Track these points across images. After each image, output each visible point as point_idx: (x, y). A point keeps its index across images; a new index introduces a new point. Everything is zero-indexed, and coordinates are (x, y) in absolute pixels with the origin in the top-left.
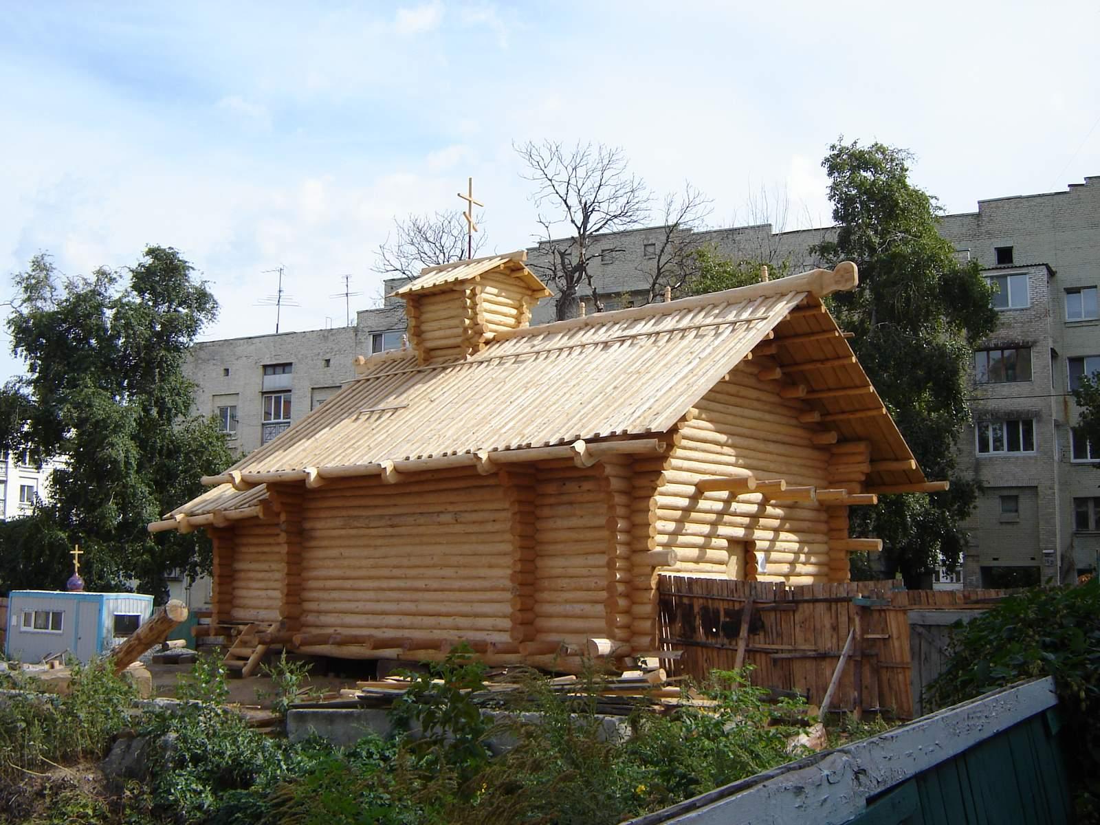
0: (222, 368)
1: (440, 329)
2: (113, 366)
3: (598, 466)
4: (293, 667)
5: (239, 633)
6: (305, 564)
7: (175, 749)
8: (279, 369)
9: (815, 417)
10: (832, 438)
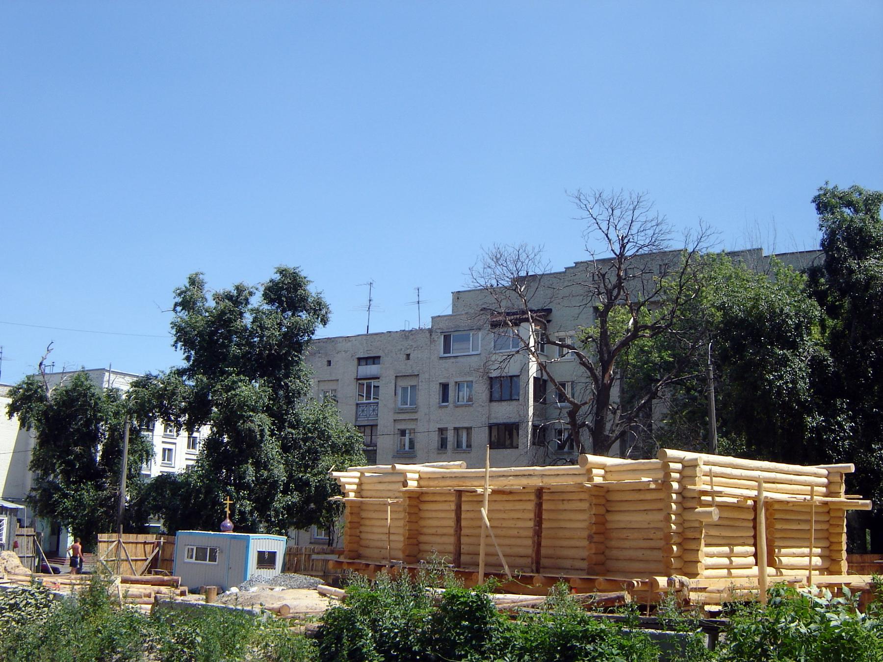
0: (326, 360)
8: (370, 361)
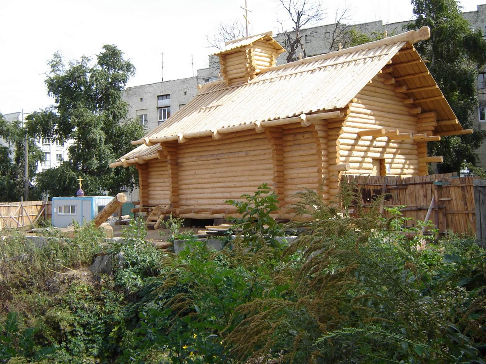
1: (235, 69)
2: (91, 98)
3: (312, 126)
4: (175, 220)
5: (152, 210)
6: (180, 178)
7: (124, 260)
8: (164, 97)
9: (411, 101)
10: (419, 110)
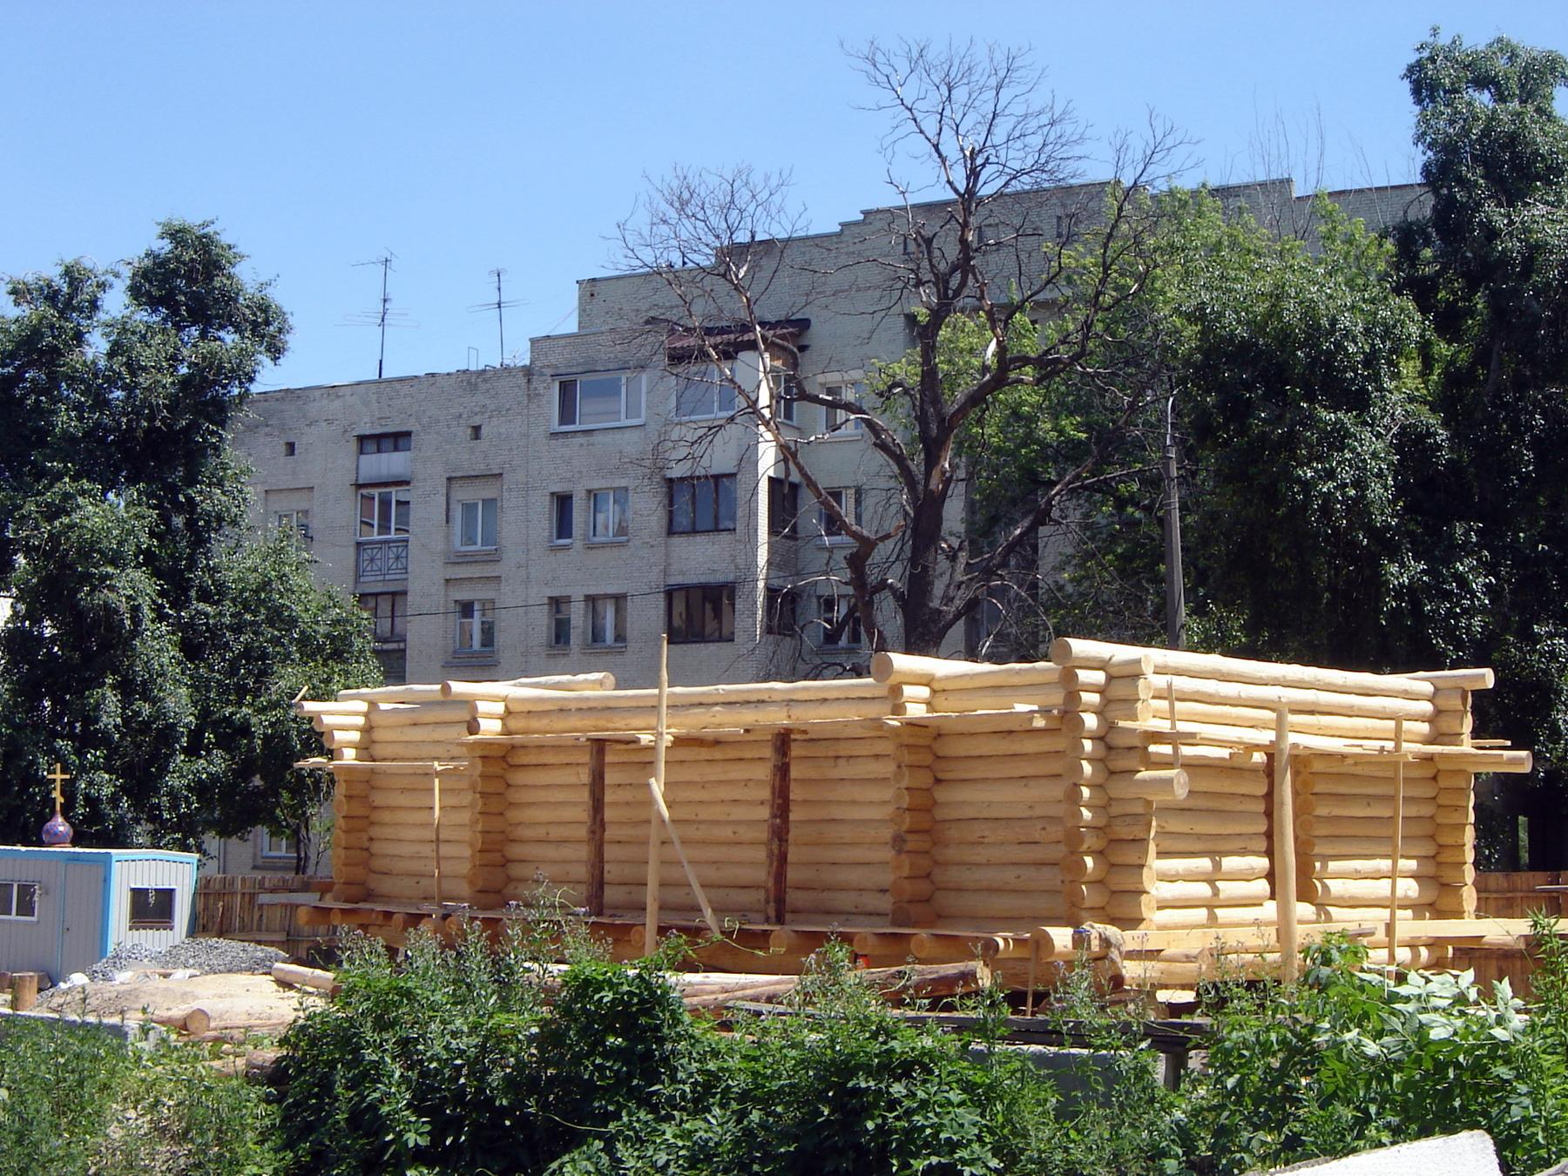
8: (389, 443)
